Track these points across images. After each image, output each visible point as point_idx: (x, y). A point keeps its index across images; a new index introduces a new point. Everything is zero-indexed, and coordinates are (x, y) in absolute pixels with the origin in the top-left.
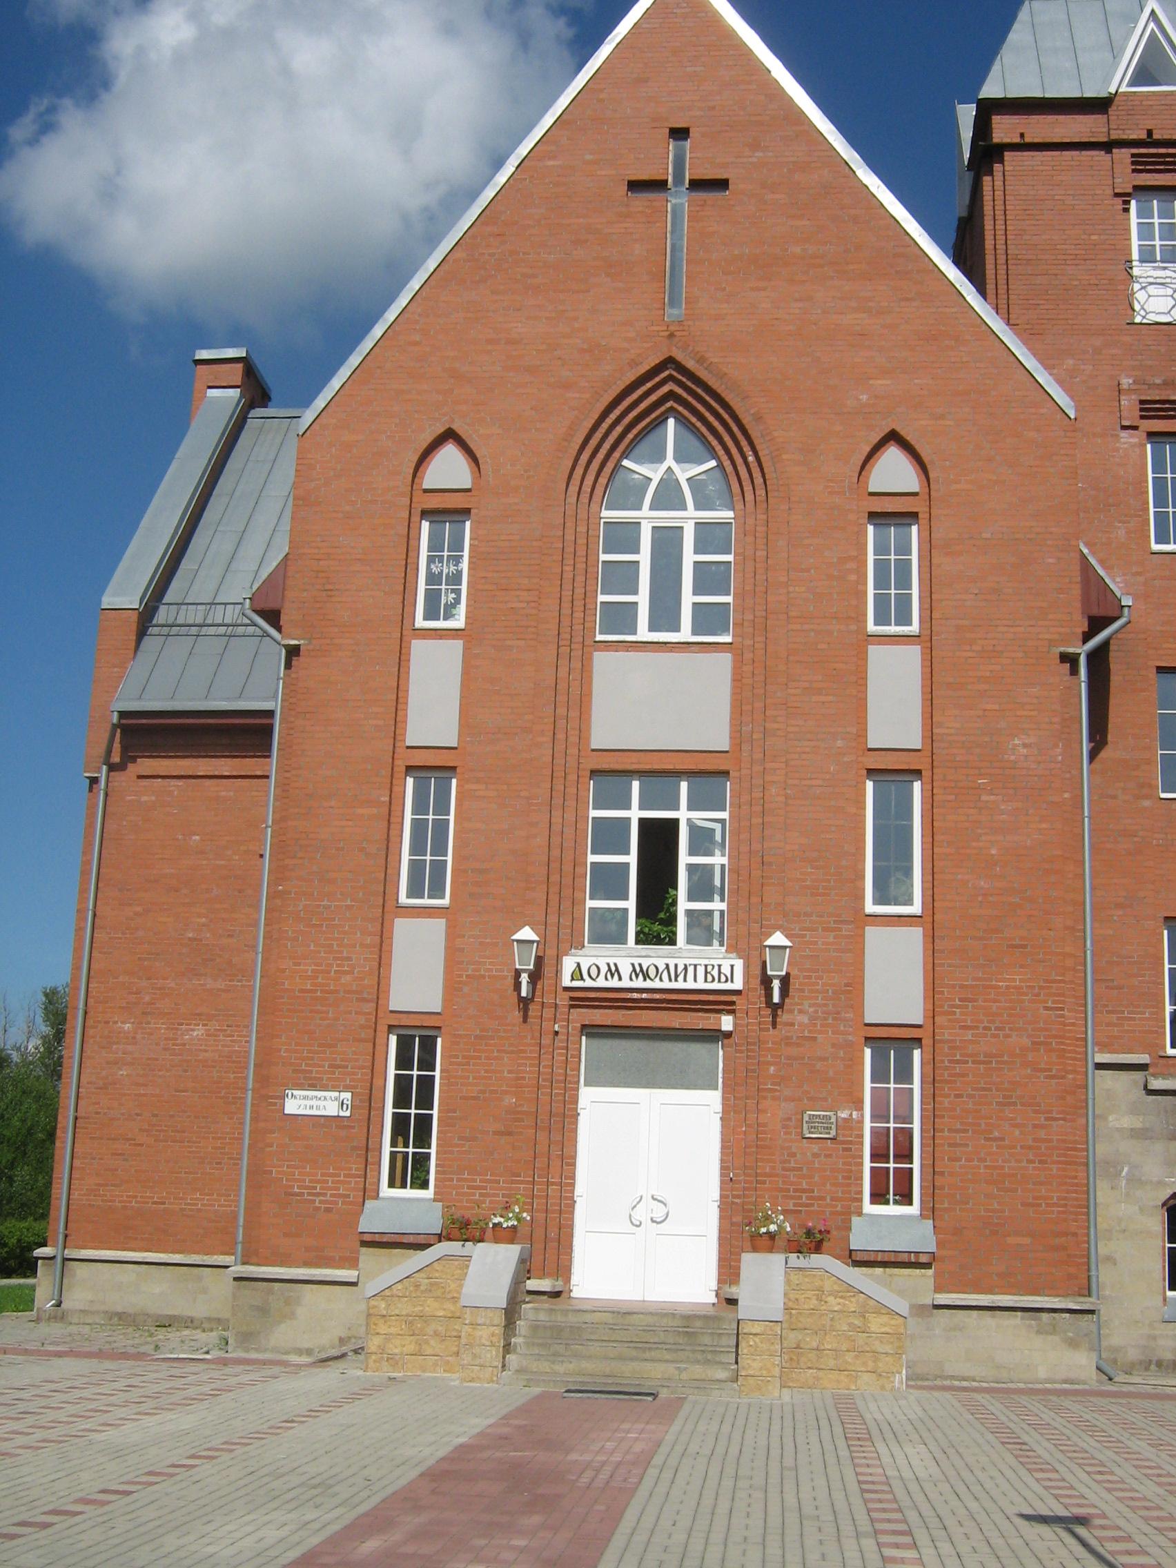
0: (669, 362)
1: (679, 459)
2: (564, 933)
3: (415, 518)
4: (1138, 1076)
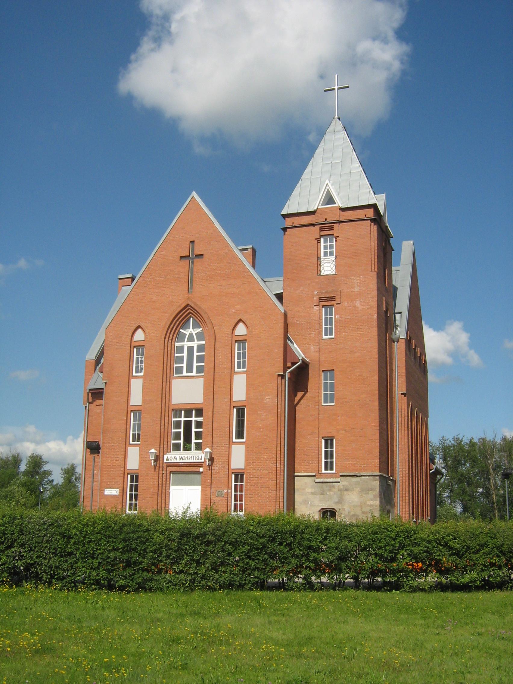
0: (188, 305)
1: (193, 328)
2: (165, 449)
3: (132, 348)
4: (313, 478)
